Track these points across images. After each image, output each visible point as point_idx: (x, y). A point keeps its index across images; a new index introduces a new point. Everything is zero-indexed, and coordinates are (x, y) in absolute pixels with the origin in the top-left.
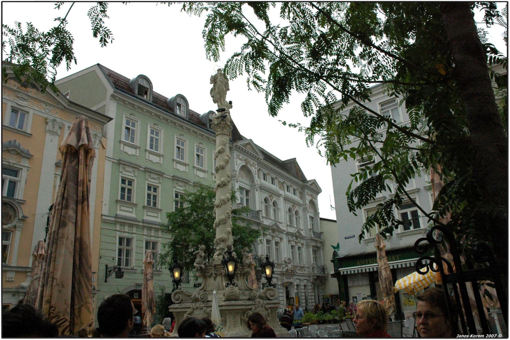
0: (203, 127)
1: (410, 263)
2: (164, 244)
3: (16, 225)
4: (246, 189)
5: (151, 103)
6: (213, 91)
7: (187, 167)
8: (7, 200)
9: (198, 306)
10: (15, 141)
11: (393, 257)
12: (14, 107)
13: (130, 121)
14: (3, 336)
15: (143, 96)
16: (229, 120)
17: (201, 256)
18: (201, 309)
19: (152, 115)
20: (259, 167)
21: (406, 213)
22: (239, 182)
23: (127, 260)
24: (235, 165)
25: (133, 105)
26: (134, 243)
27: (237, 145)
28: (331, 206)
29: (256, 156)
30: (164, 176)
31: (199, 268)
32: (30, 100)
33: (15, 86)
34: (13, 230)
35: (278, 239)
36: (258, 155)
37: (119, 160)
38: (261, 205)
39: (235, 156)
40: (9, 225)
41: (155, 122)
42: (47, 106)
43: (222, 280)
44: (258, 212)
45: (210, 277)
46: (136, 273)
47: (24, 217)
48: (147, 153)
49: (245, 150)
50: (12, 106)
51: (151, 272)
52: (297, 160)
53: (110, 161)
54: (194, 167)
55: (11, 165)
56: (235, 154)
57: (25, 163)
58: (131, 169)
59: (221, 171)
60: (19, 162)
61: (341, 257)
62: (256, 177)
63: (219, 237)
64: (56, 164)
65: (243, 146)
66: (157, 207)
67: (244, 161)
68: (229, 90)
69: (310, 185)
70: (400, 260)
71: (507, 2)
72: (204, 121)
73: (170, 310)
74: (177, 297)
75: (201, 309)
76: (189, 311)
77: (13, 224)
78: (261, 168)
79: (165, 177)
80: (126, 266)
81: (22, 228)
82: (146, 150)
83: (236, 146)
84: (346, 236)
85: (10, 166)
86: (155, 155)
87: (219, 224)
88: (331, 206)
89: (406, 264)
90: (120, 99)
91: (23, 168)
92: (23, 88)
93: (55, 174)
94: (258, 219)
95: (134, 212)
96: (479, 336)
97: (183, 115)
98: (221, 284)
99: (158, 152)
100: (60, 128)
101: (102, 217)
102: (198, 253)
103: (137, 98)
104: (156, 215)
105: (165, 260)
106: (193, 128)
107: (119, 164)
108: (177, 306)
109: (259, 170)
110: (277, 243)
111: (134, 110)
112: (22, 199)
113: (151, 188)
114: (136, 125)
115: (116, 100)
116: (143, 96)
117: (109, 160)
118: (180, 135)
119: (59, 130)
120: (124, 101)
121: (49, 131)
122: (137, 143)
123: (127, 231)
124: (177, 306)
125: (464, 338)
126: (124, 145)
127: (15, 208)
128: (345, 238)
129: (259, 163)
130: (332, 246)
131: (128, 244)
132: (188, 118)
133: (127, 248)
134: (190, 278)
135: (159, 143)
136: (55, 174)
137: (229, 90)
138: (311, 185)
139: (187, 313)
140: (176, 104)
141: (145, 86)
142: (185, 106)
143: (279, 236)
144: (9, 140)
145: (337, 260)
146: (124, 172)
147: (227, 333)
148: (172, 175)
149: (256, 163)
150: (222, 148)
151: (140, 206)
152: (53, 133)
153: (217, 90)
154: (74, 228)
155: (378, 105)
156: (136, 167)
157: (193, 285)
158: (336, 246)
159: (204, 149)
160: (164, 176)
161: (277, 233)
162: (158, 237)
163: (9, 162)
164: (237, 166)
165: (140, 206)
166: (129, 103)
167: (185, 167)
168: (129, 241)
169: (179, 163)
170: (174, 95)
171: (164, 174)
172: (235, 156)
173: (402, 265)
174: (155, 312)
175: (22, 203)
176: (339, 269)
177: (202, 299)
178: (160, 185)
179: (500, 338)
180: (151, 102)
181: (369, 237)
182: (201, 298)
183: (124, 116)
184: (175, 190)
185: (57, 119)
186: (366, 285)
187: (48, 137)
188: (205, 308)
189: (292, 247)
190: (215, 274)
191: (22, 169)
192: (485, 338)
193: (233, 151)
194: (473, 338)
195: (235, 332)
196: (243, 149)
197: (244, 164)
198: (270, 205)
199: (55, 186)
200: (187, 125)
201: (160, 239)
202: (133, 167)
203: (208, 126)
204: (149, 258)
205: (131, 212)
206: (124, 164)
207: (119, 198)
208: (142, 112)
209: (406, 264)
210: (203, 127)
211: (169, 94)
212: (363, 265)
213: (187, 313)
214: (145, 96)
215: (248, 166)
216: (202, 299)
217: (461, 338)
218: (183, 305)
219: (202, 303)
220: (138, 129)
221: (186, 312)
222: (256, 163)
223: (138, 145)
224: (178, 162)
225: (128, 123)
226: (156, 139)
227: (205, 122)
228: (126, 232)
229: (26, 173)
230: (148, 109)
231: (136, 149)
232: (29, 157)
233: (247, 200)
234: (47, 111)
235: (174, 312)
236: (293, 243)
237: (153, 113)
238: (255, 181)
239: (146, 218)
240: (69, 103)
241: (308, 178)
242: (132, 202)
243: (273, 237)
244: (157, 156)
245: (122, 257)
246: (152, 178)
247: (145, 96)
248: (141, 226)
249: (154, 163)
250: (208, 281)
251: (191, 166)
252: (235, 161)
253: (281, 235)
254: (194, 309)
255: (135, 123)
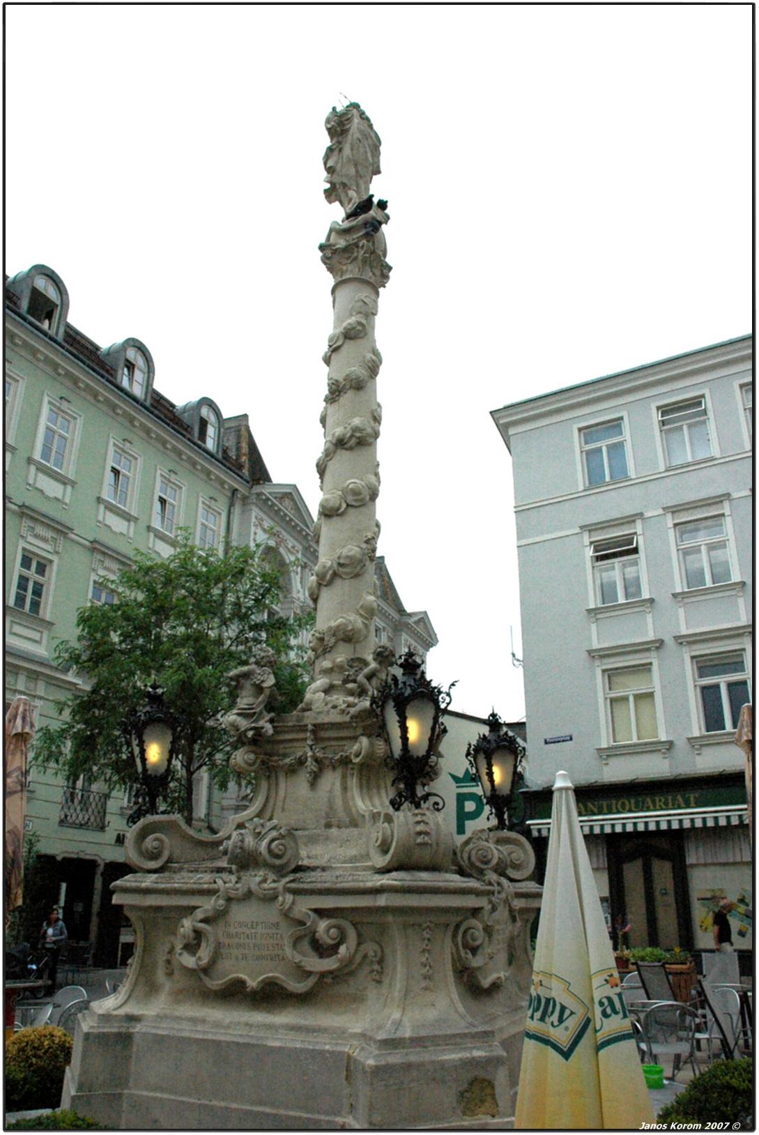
0: (185, 433)
1: (728, 818)
2: (59, 703)
6: (336, 153)
7: (132, 523)
9: (254, 887)
11: (679, 797)
15: (40, 320)
16: (383, 249)
17: (259, 689)
18: (271, 898)
20: (305, 560)
21: (717, 686)
27: (262, 494)
28: (514, 655)
29: (302, 530)
31: (250, 734)
37: (94, 542)
39: (253, 520)
41: (64, 393)
43: (345, 789)
45: (292, 770)
48: (33, 468)
49: (280, 510)
51: (20, 768)
52: (387, 562)
54: (149, 528)
58: (49, 534)
59: (347, 398)
61: (534, 789)
63: (333, 624)
65: (276, 498)
66: (41, 615)
68: (378, 172)
69: (415, 623)
70: (697, 806)
72: (186, 418)
73: (116, 899)
74: (150, 842)
75: (271, 898)
76: (208, 905)
78: (309, 563)
79: (72, 540)
82: (30, 461)
84: (549, 736)
86: (50, 476)
87: (335, 575)
88: (514, 655)
89: (716, 819)
97: (138, 391)
98: (339, 802)
102: (246, 675)
104: (36, 636)
105: (58, 746)
106: (157, 429)
108: (148, 881)
111: (147, 442)
124: (148, 881)
125: (656, 1130)
128: (546, 743)
130: (451, 775)
134: (108, 818)
137: (378, 172)
138: (417, 623)
139: (199, 914)
140: (122, 363)
142: (146, 370)
145: (521, 797)
147: (396, 1015)
148: (91, 539)
149: (299, 547)
150: (360, 323)
153: (347, 151)
155: (654, 410)
157: (115, 838)
158: (461, 776)
167: (126, 523)
169: (111, 510)
170: (119, 339)
171: (71, 530)
172: (253, 520)
173: (704, 820)
174: (20, 902)
176: (528, 822)
177: (278, 857)
179: (735, 1131)
181: (612, 743)
182: (270, 851)
184: (93, 577)
186: (604, 869)
188: (289, 898)
190: (316, 760)
192: (702, 1130)
193: (249, 507)
194: (676, 1131)
195: (431, 1015)
196: (274, 504)
200: (142, 419)
201: (38, 703)
202: (54, 528)
203: (196, 433)
204: (19, 721)
205: (36, 641)
208: (33, 360)
209: (716, 819)
210: (185, 433)
211: (104, 337)
212: (594, 814)
213: (199, 914)
214: (47, 322)
215: (282, 550)
216: (278, 857)
218: (183, 879)
219: (271, 876)
221: (195, 908)
222: (300, 547)
223: (71, 476)
224: (110, 508)
235: (133, 907)
238: (294, 590)
241: (409, 608)
244: (56, 480)
246: (36, 536)
247: (47, 322)
250: (282, 793)
252: (252, 534)
254: (229, 900)
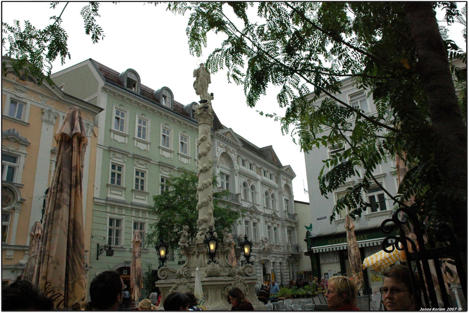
0: (187, 117)
1: (377, 243)
2: (150, 225)
3: (14, 208)
4: (226, 174)
5: (139, 95)
6: (196, 84)
7: (172, 153)
8: (6, 184)
9: (182, 282)
10: (14, 130)
11: (362, 236)
12: (13, 99)
13: (119, 111)
14: (3, 310)
15: (131, 89)
16: (211, 110)
17: (185, 236)
18: (185, 284)
19: (140, 106)
20: (238, 154)
21: (374, 196)
22: (219, 168)
23: (117, 240)
24: (216, 152)
25: (123, 97)
26: (123, 224)
27: (218, 134)
28: (305, 190)
29: (235, 144)
30: (151, 162)
31: (183, 247)
32: (27, 92)
33: (14, 79)
34: (12, 212)
35: (255, 220)
36: (237, 142)
37: (110, 147)
38: (240, 189)
39: (216, 144)
40: (8, 207)
41: (143, 112)
42: (43, 97)
43: (204, 258)
44: (237, 195)
45: (193, 255)
46: (125, 251)
47: (22, 199)
48: (135, 141)
49: (226, 138)
50: (11, 98)
51: (139, 251)
52: (273, 147)
53: (102, 148)
54: (178, 154)
55: (10, 152)
56: (216, 142)
57: (23, 150)
58: (120, 156)
59: (203, 158)
60: (18, 149)
61: (314, 236)
62: (235, 163)
63: (202, 218)
64: (51, 151)
65: (224, 134)
66: (144, 191)
67: (224, 148)
68: (210, 82)
69: (285, 170)
70: (368, 239)
71: (467, 2)
72: (188, 112)
73: (156, 286)
74: (162, 273)
75: (185, 284)
76: (174, 286)
77: (12, 206)
78: (240, 155)
79: (152, 163)
80: (116, 245)
81: (20, 210)
82: (134, 138)
83: (217, 134)
84: (318, 217)
85: (9, 153)
86: (142, 143)
87: (201, 206)
88: (305, 190)
89: (373, 243)
90: (110, 91)
91: (22, 155)
92: (22, 81)
93: (51, 160)
94: (238, 201)
95: (123, 195)
96: (441, 309)
97: (169, 106)
98: (203, 261)
99: (146, 140)
100: (56, 118)
101: (93, 200)
102: (182, 233)
103: (126, 90)
104: (143, 198)
105: (152, 239)
106: (177, 118)
107: (110, 151)
108: (162, 281)
109: (238, 157)
110: (254, 224)
111: (123, 101)
112: (20, 183)
113: (139, 173)
114: (125, 115)
115: (107, 92)
116: (131, 89)
117: (100, 148)
118: (166, 124)
119: (54, 120)
120: (114, 93)
121: (45, 120)
122: (126, 131)
123: (117, 213)
124: (162, 281)
125: (426, 311)
126: (114, 133)
127: (14, 191)
128: (318, 219)
129: (239, 150)
130: (305, 226)
131: (118, 225)
132: (173, 108)
133: (117, 228)
134: (175, 256)
135: (146, 131)
136: (51, 160)
137: (210, 82)
138: (286, 170)
139: (172, 288)
140: (162, 96)
141: (134, 79)
142: (171, 97)
143: (256, 217)
144: (8, 129)
145: (310, 239)
146: (114, 159)
147: (208, 306)
148: (158, 161)
149: (235, 150)
150: (204, 137)
151: (129, 190)
152: (49, 122)
153: (199, 83)
154: (68, 210)
155: (347, 96)
156: (125, 154)
157: (178, 262)
158: (309, 226)
159: (188, 137)
160: (151, 162)
161: (255, 215)
162: (145, 218)
163: (8, 150)
164: (218, 153)
165: (129, 190)
166: (119, 95)
167: (170, 154)
168: (119, 222)
169: (165, 150)
170: (160, 88)
171: (151, 160)
172: (216, 144)
173: (369, 244)
174: (142, 287)
175: (20, 186)
176: (312, 248)
177: (186, 275)
178: (147, 170)
179: (459, 311)
180: (139, 94)
181: (340, 218)
182: (184, 274)
183: (114, 106)
184: (161, 174)
185: (52, 110)
186: (337, 262)
187: (45, 126)
188: (189, 284)
189: (269, 227)
190: (198, 252)
191: (20, 156)
192: (446, 311)
193: (214, 139)
194: (435, 311)
195: (216, 306)
196: (223, 137)
197: (225, 151)
198: (248, 189)
199: (50, 171)
200: (172, 115)
201: (147, 220)
202: (122, 154)
203: (191, 116)
204: (137, 238)
205: (121, 195)
206: (114, 151)
207: (110, 183)
208: (131, 103)
209: (373, 243)
210: (187, 117)
211: (155, 86)
212: (334, 244)
213: (172, 288)
214: (134, 88)
215: (228, 153)
216: (186, 275)
217: (424, 311)
218: (168, 281)
219: (185, 279)
220: (127, 119)
221: (171, 287)
222: (236, 150)
223: (127, 133)
224: (164, 149)
225: (117, 113)
226: (143, 128)
227: (188, 113)
228: (116, 214)
229: (24, 160)
230: (136, 101)
231: (125, 137)
232: (26, 144)
233: (227, 184)
234: (43, 102)
235: (160, 287)
236: (270, 224)
237: (141, 104)
238: (235, 167)
239: (134, 201)
240: (63, 95)
241: (284, 164)
242: (121, 186)
243: (251, 218)
244: (144, 143)
245: (112, 237)
246: (140, 164)
247: (134, 88)
248: (130, 208)
249: (142, 150)
250: (191, 259)
251: (176, 153)
252: (216, 149)
253: (258, 217)
254: (178, 285)
255: (124, 113)
